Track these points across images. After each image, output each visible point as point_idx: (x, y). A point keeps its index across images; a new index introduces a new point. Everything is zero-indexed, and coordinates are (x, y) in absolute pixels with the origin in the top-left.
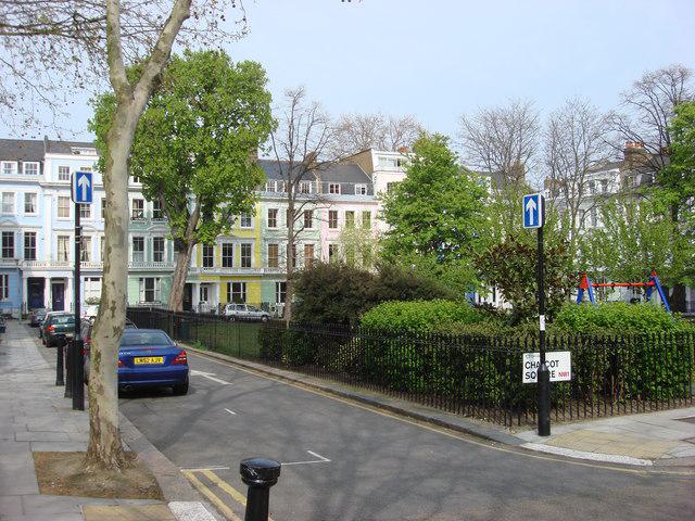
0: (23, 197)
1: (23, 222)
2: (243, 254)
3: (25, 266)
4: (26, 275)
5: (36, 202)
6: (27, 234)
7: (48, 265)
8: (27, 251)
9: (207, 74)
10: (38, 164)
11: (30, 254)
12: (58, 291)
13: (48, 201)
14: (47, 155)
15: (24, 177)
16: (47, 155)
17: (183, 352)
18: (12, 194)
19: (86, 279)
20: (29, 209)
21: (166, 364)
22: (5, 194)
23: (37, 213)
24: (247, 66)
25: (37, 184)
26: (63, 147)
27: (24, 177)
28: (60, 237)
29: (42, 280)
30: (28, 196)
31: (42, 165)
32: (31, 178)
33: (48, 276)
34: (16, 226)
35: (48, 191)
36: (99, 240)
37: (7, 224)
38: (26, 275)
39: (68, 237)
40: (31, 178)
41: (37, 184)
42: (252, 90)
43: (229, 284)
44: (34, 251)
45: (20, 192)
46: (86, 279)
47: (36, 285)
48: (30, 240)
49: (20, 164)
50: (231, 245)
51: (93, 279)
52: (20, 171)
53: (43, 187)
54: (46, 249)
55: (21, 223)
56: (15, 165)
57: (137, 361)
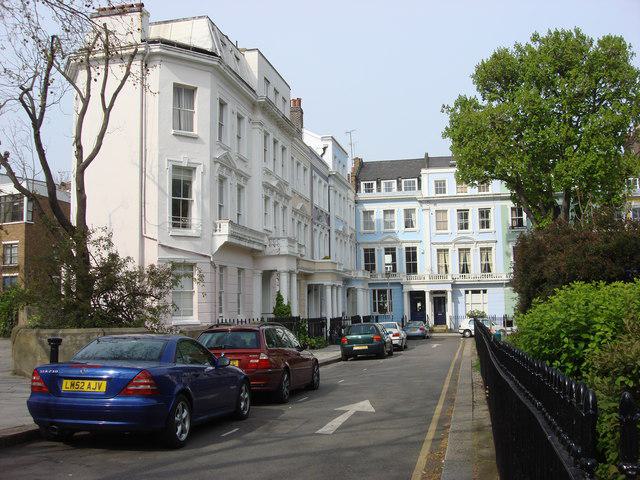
0: (403, 214)
1: (404, 237)
2: (408, 258)
3: (405, 280)
4: (407, 289)
5: (416, 217)
6: (408, 249)
7: (427, 279)
8: (408, 266)
9: (558, 57)
10: (416, 180)
11: (412, 268)
12: (440, 304)
13: (426, 215)
14: (423, 171)
15: (404, 194)
16: (423, 171)
17: (239, 367)
18: (392, 211)
19: (467, 292)
20: (409, 224)
21: (110, 392)
22: (385, 212)
23: (492, 228)
24: (606, 42)
25: (415, 199)
26: (429, 162)
27: (404, 194)
28: (482, 249)
29: (422, 293)
30: (408, 213)
31: (419, 181)
32: (409, 194)
33: (427, 289)
34: (398, 242)
35: (425, 206)
36: (457, 252)
37: (388, 240)
38: (407, 289)
39: (469, 249)
40: (409, 194)
41: (415, 199)
42: (614, 66)
43: (374, 291)
44: (415, 266)
45: (399, 208)
46: (467, 292)
47: (417, 297)
48: (411, 255)
49: (399, 182)
50: (373, 250)
51: (474, 292)
52: (399, 188)
53: (420, 202)
54: (426, 262)
55: (401, 239)
56: (394, 183)
57: (66, 386)
